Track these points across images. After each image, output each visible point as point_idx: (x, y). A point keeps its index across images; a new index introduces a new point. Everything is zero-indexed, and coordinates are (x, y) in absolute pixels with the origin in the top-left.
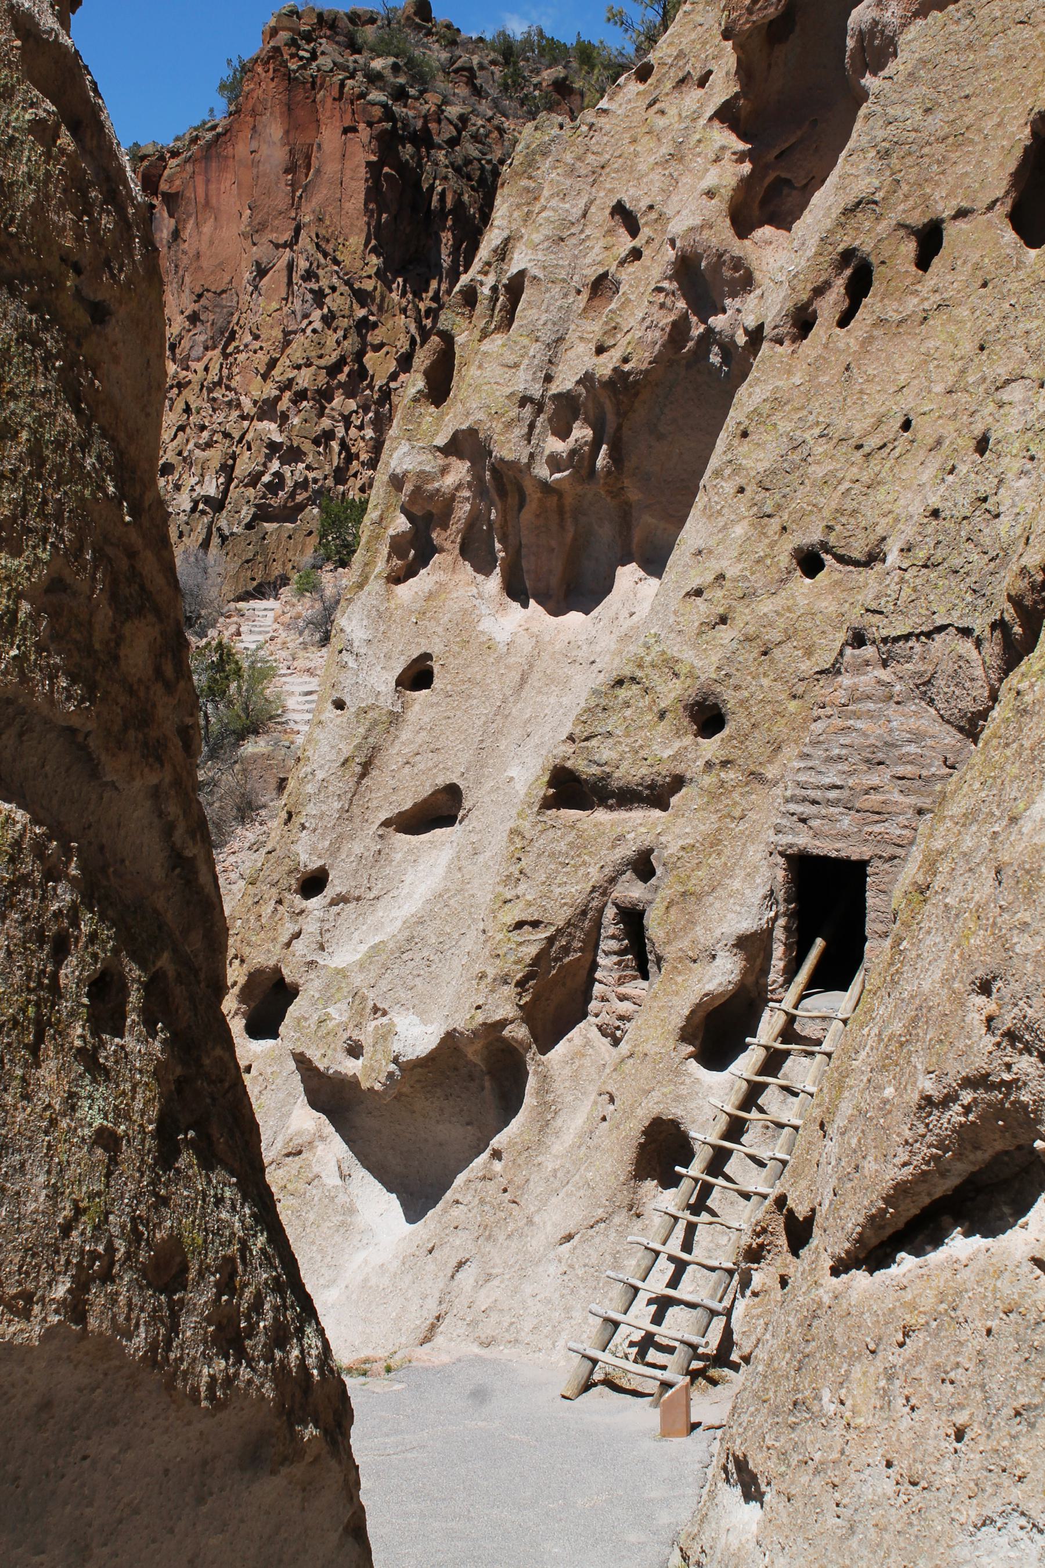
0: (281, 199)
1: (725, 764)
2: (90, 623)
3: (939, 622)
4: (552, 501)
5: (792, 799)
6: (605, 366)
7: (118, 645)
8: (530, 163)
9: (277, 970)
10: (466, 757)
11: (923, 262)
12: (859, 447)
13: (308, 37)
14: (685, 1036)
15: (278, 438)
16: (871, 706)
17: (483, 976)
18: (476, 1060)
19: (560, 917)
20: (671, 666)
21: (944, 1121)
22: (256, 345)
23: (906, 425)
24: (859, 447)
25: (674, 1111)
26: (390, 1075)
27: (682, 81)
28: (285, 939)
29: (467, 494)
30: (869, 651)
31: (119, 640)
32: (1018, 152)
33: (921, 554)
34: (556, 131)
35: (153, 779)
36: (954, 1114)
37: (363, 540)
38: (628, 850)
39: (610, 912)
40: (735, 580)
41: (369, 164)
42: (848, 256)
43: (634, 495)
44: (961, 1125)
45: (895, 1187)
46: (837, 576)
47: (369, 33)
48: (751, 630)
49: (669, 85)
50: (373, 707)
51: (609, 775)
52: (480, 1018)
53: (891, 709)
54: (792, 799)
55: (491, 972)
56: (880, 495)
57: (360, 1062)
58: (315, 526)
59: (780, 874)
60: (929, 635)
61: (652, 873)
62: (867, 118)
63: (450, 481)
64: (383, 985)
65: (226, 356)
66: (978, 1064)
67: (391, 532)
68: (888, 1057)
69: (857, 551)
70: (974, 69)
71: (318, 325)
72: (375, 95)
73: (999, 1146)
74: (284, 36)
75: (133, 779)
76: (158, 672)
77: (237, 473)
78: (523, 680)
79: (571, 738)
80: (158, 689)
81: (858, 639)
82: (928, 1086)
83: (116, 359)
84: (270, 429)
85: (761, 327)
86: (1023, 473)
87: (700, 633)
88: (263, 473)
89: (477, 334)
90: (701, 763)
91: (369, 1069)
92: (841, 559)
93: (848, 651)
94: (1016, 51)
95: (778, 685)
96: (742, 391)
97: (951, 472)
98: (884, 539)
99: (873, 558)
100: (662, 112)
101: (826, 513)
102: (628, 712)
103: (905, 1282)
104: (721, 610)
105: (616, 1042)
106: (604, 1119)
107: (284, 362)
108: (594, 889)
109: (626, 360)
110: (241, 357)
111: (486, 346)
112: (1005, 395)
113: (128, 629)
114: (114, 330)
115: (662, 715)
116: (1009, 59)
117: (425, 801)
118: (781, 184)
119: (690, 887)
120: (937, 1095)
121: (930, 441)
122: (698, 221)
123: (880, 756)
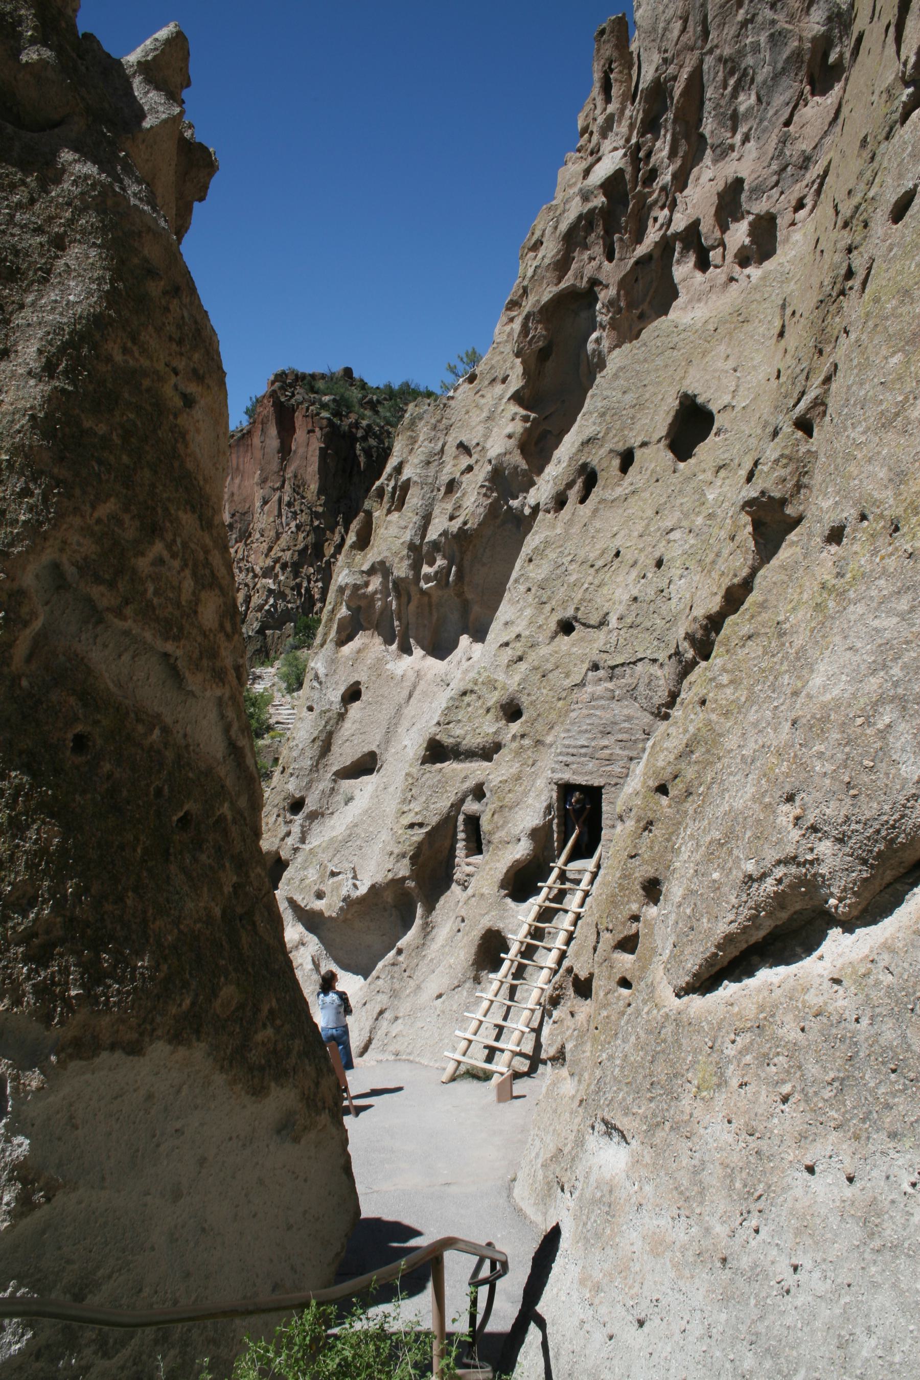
0: (275, 465)
1: (523, 736)
2: (180, 588)
3: (640, 656)
4: (426, 599)
5: (561, 754)
6: (455, 525)
7: (197, 604)
8: (413, 423)
9: (277, 853)
10: (378, 737)
11: (624, 469)
12: (592, 566)
13: (290, 385)
14: (503, 885)
15: (273, 587)
16: (602, 702)
17: (391, 853)
18: (389, 900)
19: (434, 820)
20: (492, 685)
21: (761, 890)
22: (262, 539)
23: (617, 554)
24: (592, 566)
25: (500, 925)
26: (341, 909)
27: (494, 380)
28: (281, 835)
29: (379, 596)
30: (601, 673)
31: (197, 601)
32: (672, 413)
33: (629, 621)
34: (426, 407)
35: (218, 692)
36: (769, 886)
37: (323, 621)
38: (470, 783)
39: (461, 818)
40: (526, 637)
41: (321, 449)
42: (584, 466)
43: (469, 596)
44: (775, 893)
45: (725, 938)
46: (582, 634)
47: (321, 385)
48: (536, 663)
49: (487, 383)
50: (329, 710)
51: (460, 743)
52: (390, 876)
53: (614, 704)
54: (561, 754)
55: (396, 851)
56: (605, 590)
57: (324, 901)
58: (291, 632)
59: (555, 795)
60: (634, 663)
61: (484, 795)
62: (593, 396)
63: (371, 589)
64: (336, 860)
65: (246, 545)
66: (790, 850)
67: (338, 616)
68: (712, 854)
69: (594, 620)
70: (648, 372)
71: (294, 529)
72: (325, 414)
73: (798, 907)
74: (277, 384)
75: (206, 690)
76: (222, 627)
77: (252, 605)
78: (410, 696)
79: (438, 724)
80: (221, 637)
81: (595, 667)
82: (750, 867)
83: (198, 431)
84: (270, 583)
85: (538, 504)
86: (681, 577)
87: (508, 666)
88: (264, 605)
89: (385, 511)
90: (510, 736)
91: (330, 906)
92: (584, 624)
93: (590, 673)
94: (670, 362)
95: (551, 693)
96: (529, 537)
97: (644, 577)
98: (607, 614)
99: (603, 623)
100: (483, 396)
101: (576, 601)
102: (470, 709)
103: (732, 1000)
104: (519, 653)
105: (466, 888)
106: (459, 931)
107: (276, 548)
108: (452, 806)
109: (465, 523)
110: (255, 545)
111: (390, 517)
112: (672, 536)
113: (203, 595)
114: (198, 413)
115: (488, 711)
116: (666, 366)
117: (358, 760)
118: (544, 435)
119: (505, 803)
120: (756, 875)
121: (631, 562)
122: (503, 451)
123: (609, 729)
